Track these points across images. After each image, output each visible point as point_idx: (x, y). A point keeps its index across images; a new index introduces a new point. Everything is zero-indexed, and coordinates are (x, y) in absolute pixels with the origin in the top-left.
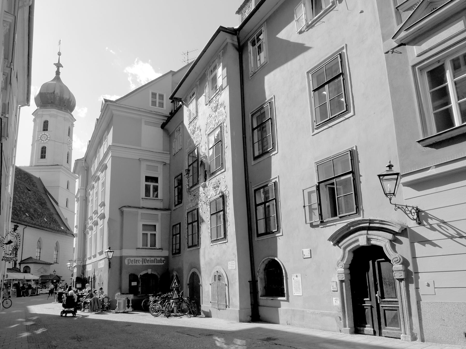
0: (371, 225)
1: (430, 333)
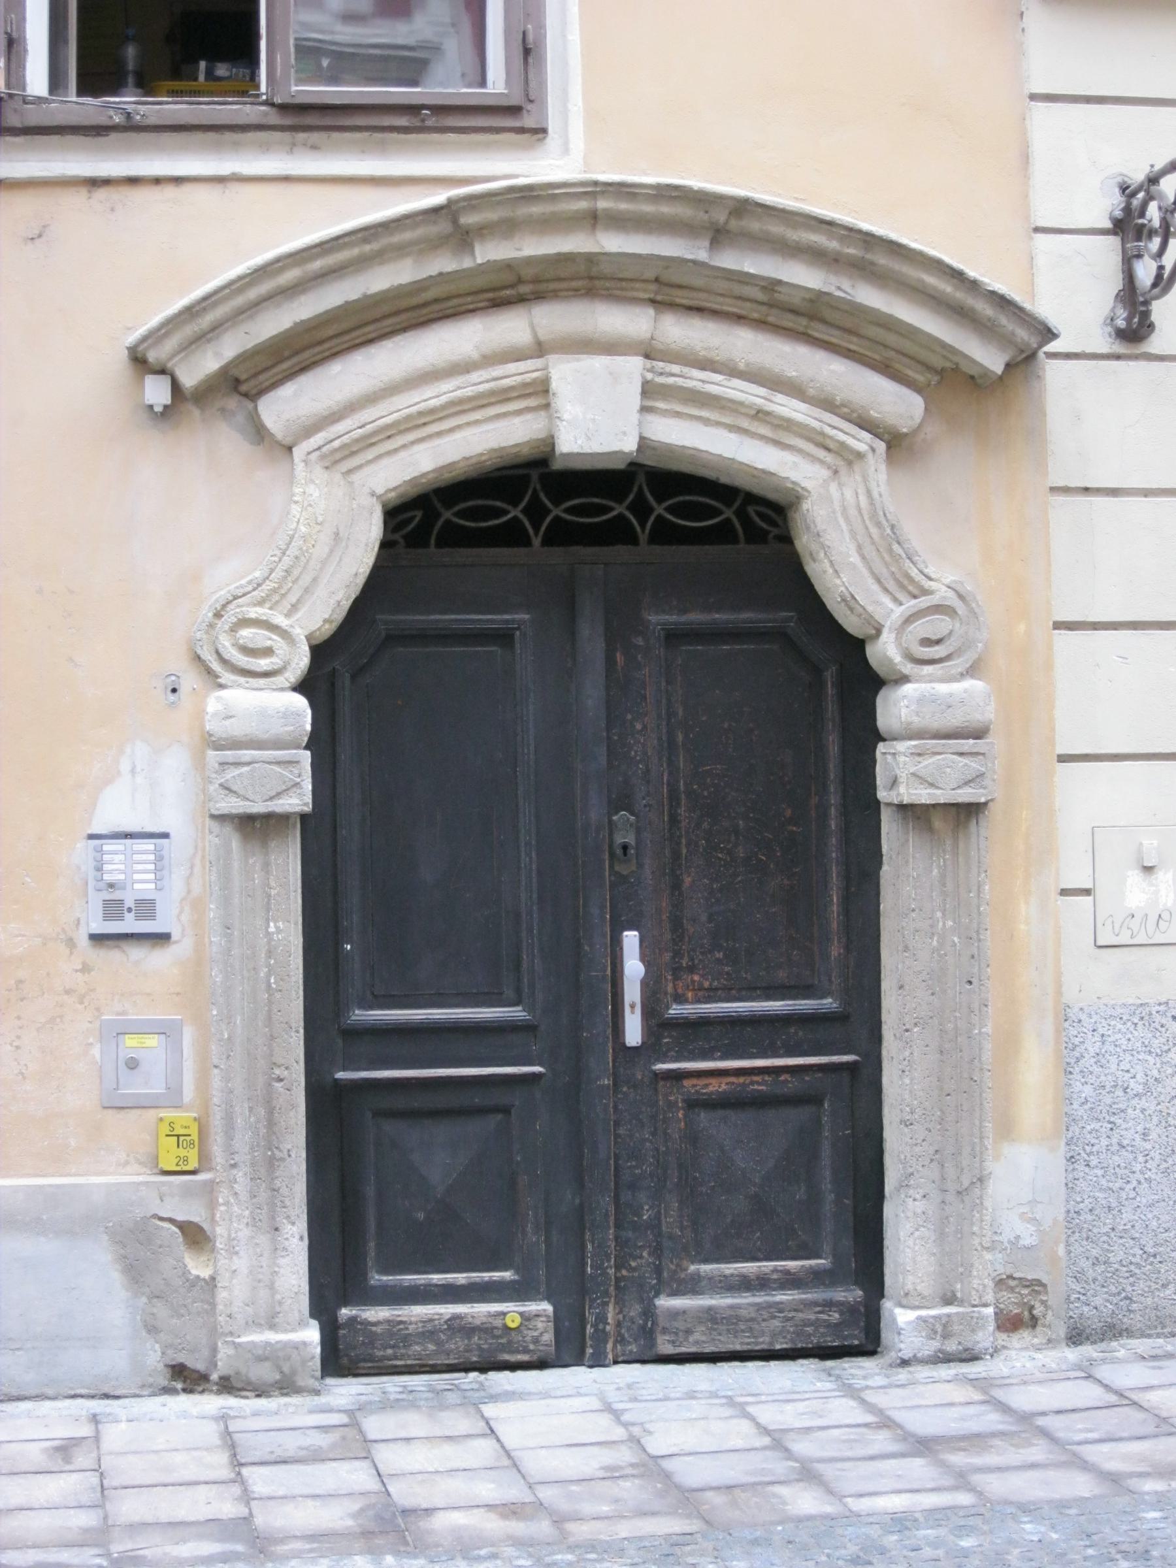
0: (730, 260)
1: (1138, 1266)
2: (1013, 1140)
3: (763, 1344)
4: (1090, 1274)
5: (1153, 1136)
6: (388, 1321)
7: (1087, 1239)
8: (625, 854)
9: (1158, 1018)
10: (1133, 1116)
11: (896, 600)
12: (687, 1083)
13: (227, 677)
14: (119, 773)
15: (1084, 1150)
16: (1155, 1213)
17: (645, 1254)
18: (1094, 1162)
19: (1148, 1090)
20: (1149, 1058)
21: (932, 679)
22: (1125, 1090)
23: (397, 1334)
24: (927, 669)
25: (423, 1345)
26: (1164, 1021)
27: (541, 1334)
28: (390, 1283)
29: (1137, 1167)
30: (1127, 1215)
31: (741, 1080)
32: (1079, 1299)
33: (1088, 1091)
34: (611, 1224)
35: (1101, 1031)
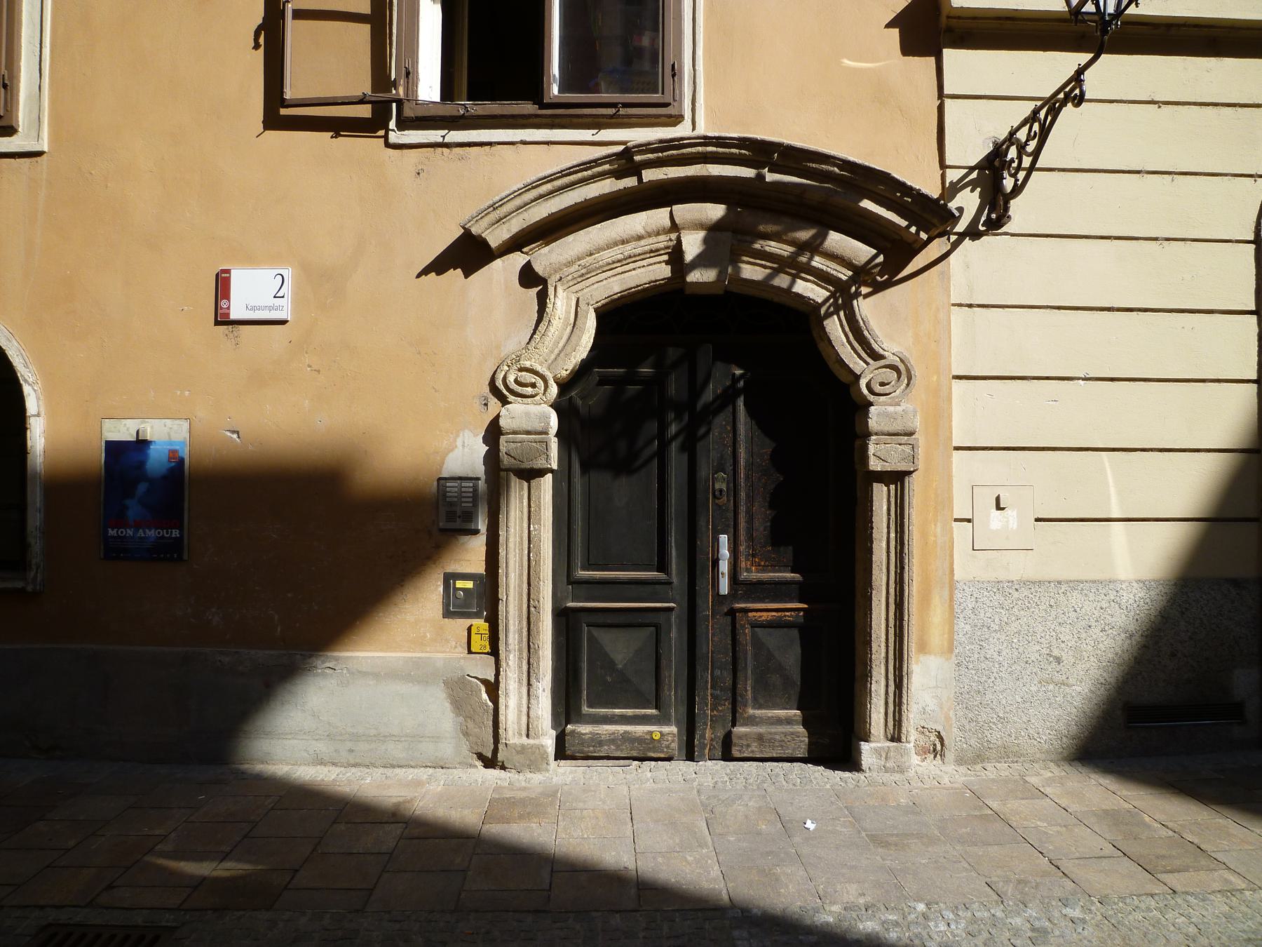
2: (926, 653)
3: (788, 753)
4: (967, 727)
5: (1004, 653)
6: (591, 733)
7: (966, 707)
8: (721, 494)
9: (1007, 590)
10: (992, 642)
11: (867, 364)
12: (750, 614)
13: (511, 398)
14: (456, 447)
15: (965, 659)
16: (1004, 695)
17: (727, 704)
18: (970, 667)
19: (1001, 629)
20: (1002, 611)
21: (885, 404)
22: (988, 628)
23: (598, 741)
24: (882, 398)
25: (609, 746)
26: (1011, 591)
27: (670, 744)
28: (593, 713)
29: (995, 670)
30: (989, 696)
31: (780, 614)
32: (961, 740)
33: (968, 627)
34: (709, 687)
35: (975, 595)
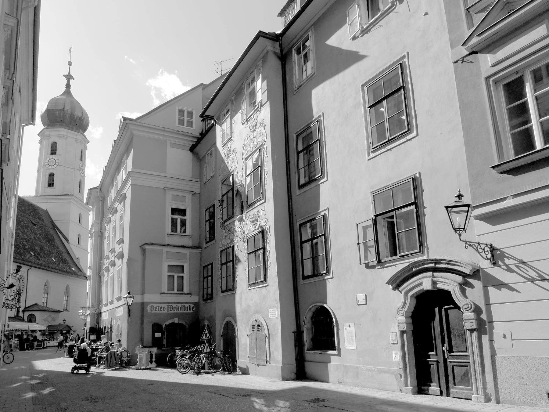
0: (437, 266)
